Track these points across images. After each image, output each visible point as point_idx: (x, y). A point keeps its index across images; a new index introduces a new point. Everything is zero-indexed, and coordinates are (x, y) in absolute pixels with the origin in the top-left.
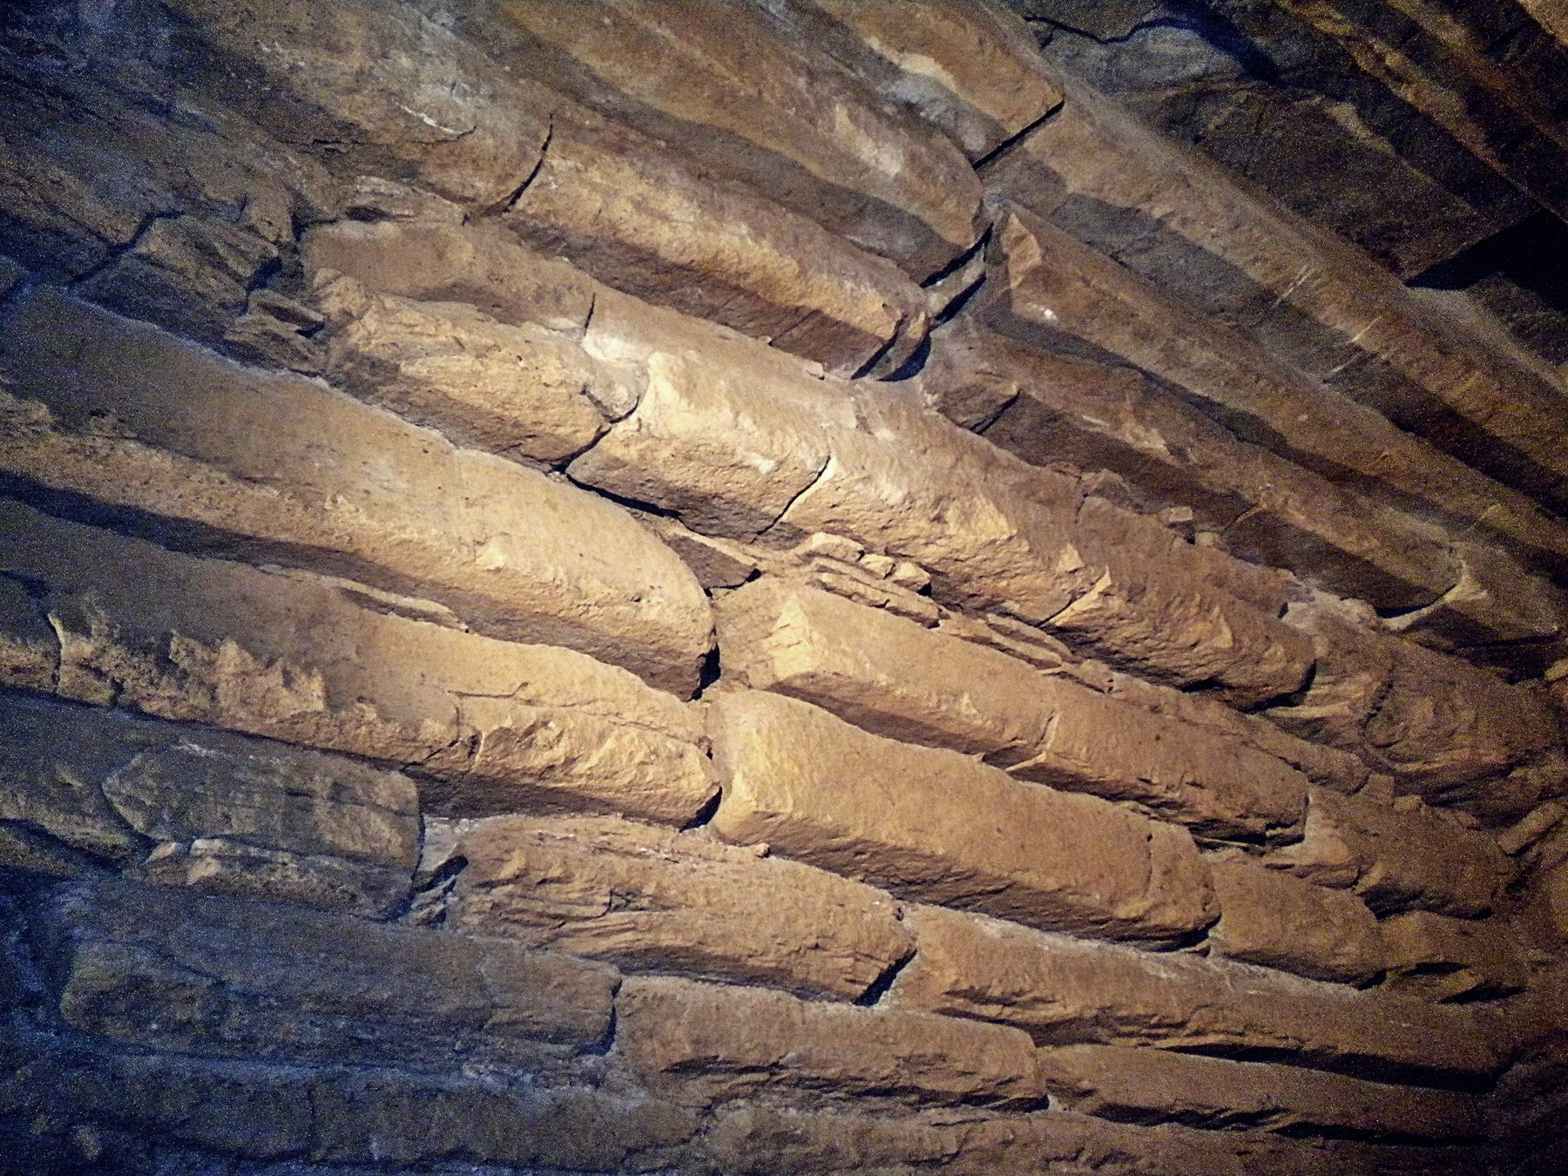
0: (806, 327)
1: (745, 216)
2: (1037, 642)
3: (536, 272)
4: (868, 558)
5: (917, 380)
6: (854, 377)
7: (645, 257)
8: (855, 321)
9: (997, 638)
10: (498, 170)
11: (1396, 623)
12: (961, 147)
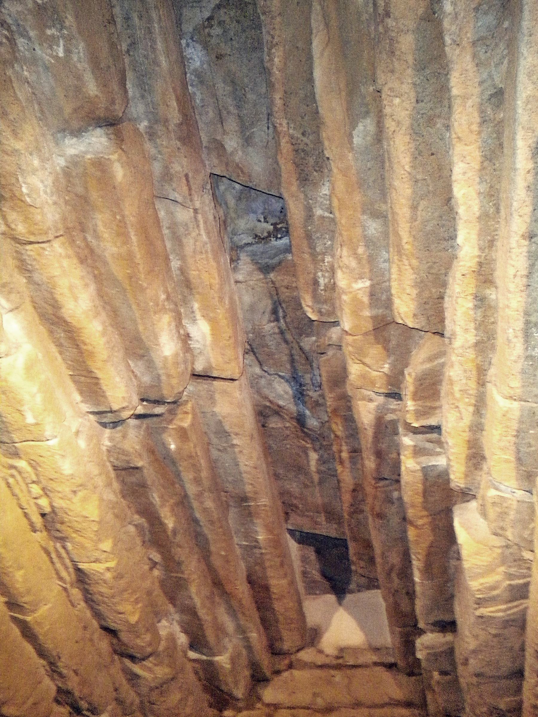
0: (89, 381)
1: (103, 323)
2: (66, 568)
3: (11, 276)
4: (34, 486)
5: (107, 432)
6: (88, 412)
7: (56, 306)
8: (108, 394)
9: (53, 555)
10: (32, 229)
11: (192, 655)
12: (193, 363)
